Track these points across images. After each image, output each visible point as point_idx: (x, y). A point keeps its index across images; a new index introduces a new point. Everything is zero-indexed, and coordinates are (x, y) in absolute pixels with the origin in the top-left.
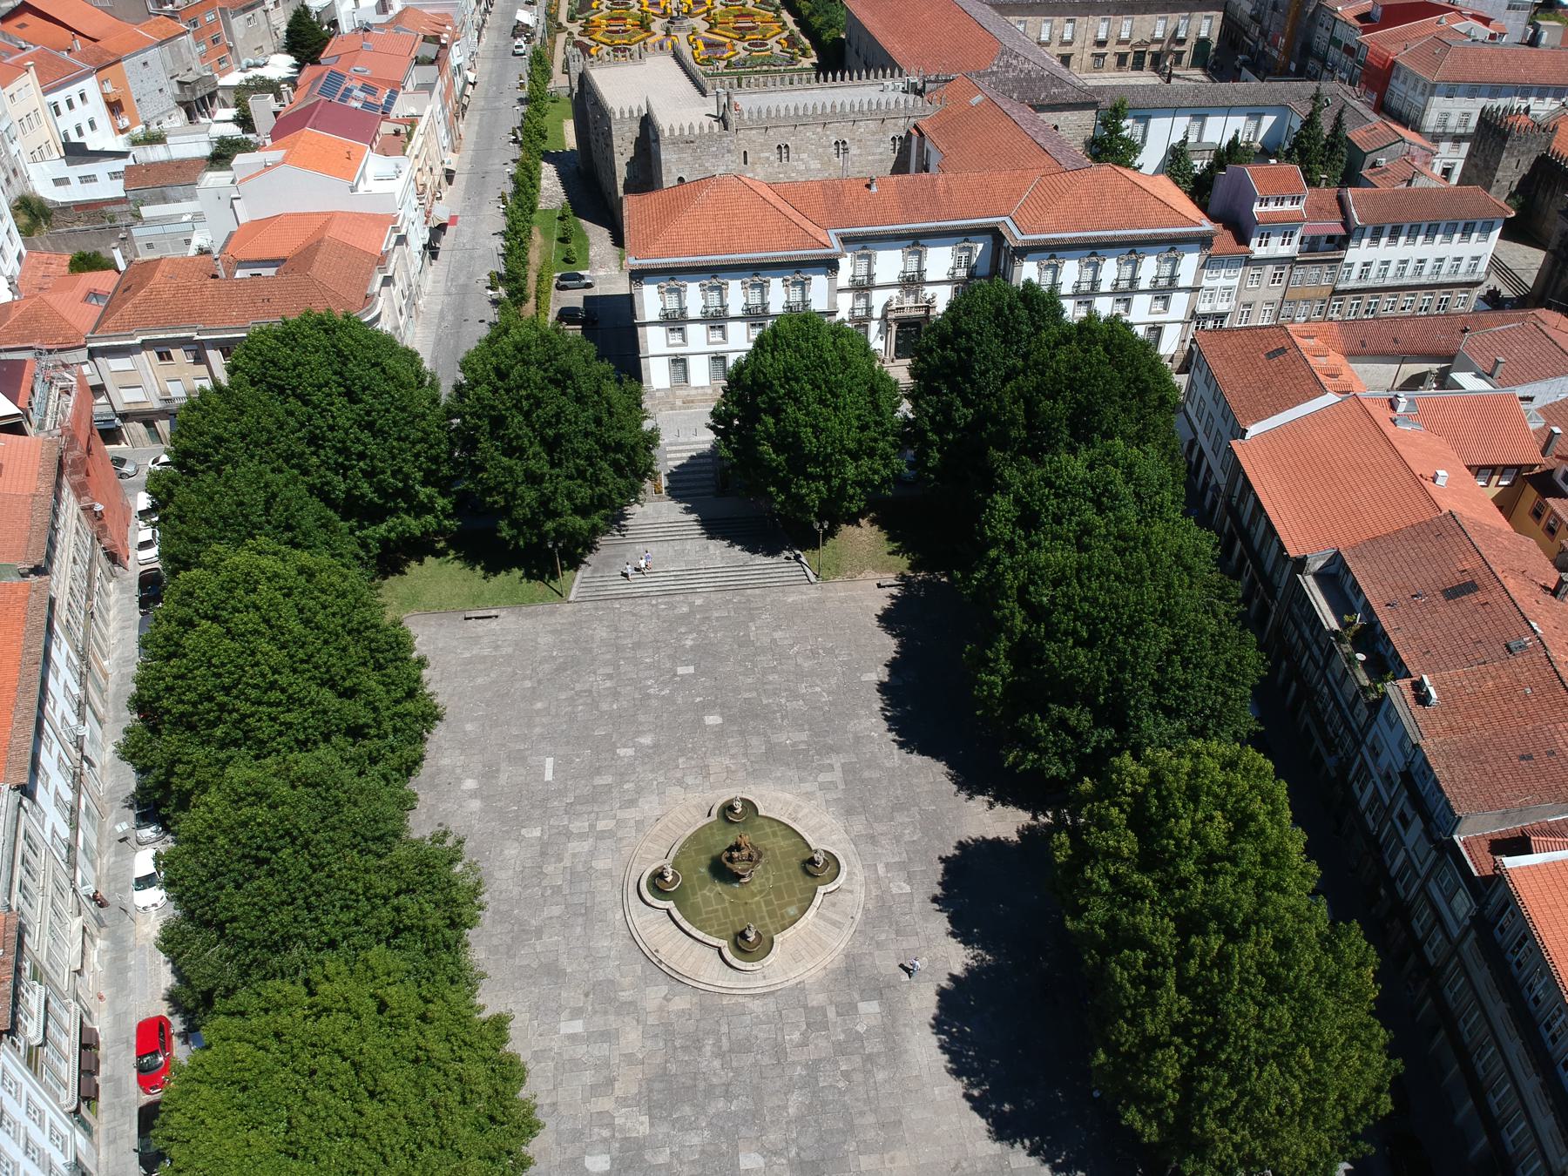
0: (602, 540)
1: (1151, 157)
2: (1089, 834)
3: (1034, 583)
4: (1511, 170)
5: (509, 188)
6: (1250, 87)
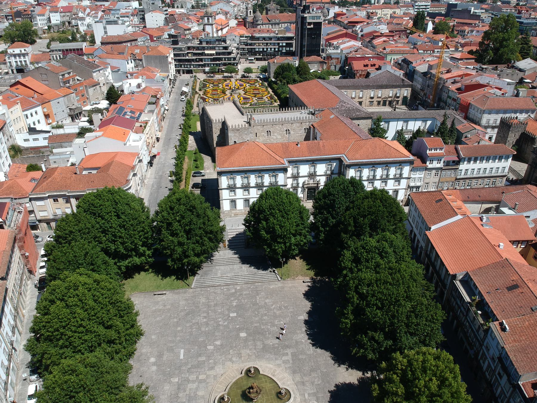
0: (204, 265)
1: (391, 134)
2: (385, 385)
3: (361, 285)
4: (513, 137)
5: (178, 143)
6: (422, 112)
